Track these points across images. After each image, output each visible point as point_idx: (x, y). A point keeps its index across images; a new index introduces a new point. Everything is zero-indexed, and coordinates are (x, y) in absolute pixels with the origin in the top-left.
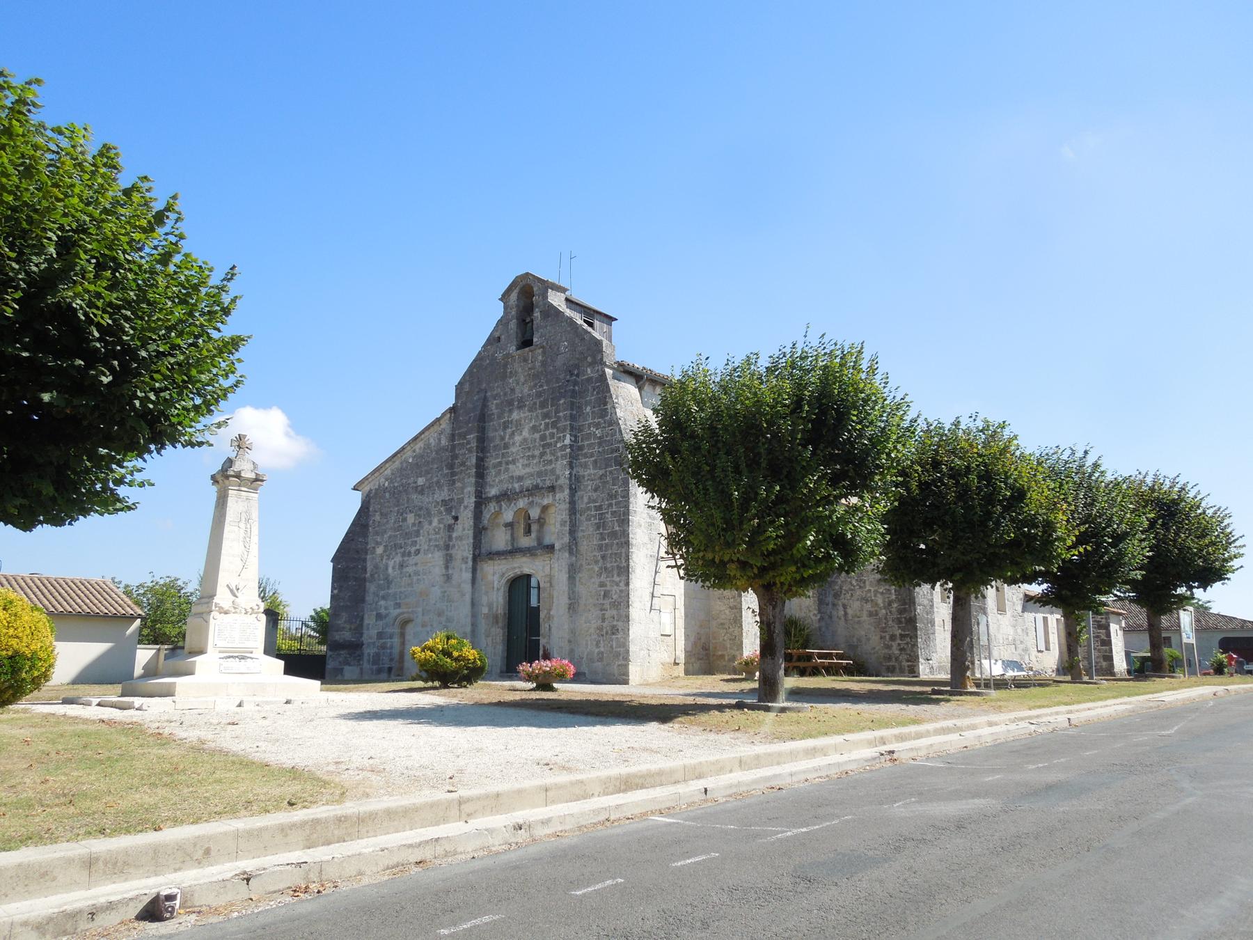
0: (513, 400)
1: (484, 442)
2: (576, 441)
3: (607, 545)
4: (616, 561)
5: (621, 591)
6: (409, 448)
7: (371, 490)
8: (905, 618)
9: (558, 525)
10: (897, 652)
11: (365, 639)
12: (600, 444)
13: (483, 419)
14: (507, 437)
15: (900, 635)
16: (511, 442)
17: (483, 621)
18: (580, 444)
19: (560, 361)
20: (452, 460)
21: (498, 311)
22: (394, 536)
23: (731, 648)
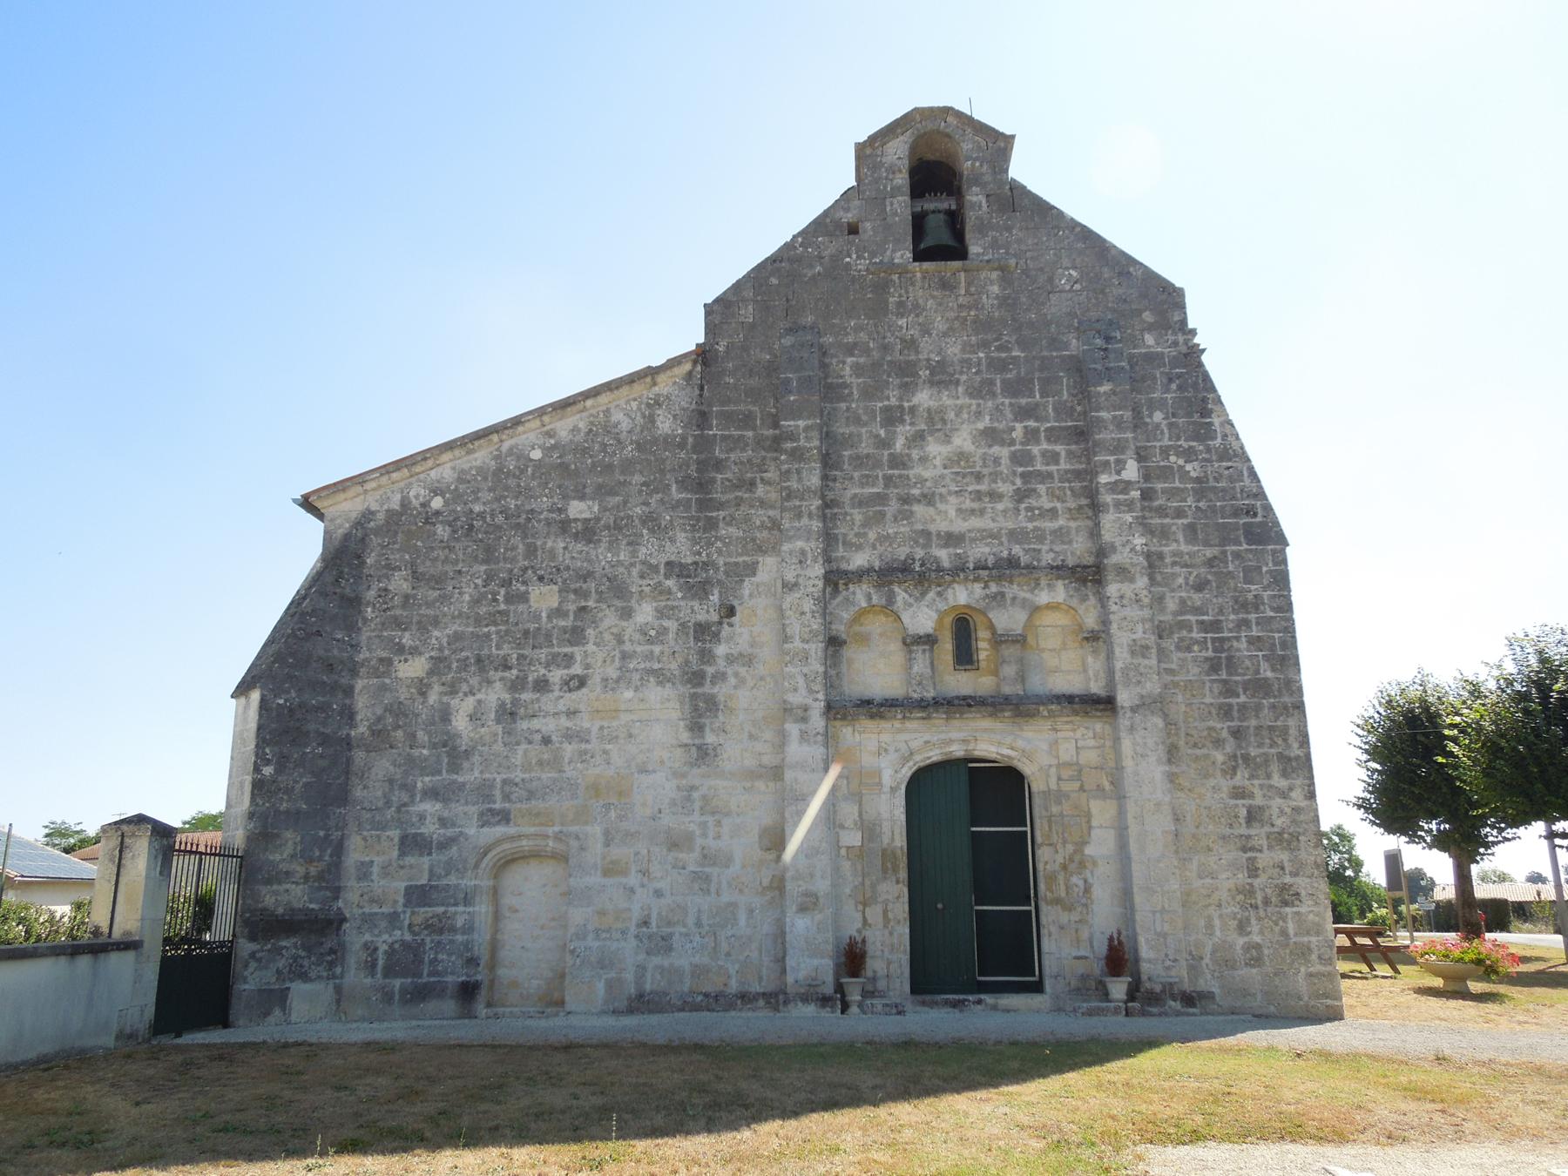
3: (1243, 708)
5: (1297, 810)
11: (352, 900)
16: (915, 454)
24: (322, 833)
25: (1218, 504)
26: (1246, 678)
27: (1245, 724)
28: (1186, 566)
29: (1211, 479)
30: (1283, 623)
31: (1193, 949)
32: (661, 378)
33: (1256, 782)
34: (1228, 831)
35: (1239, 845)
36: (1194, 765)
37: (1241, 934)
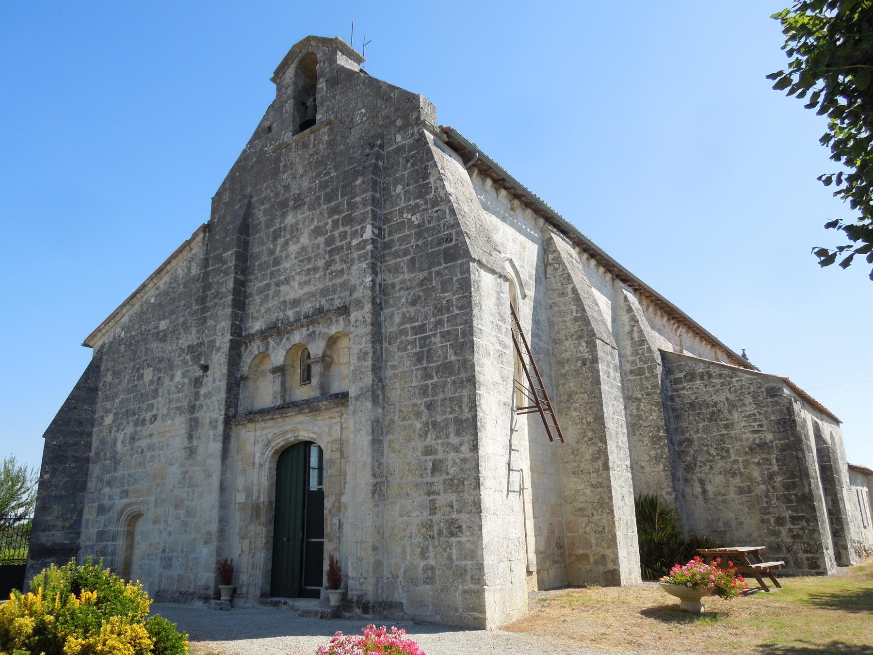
0: (287, 200)
1: (246, 261)
2: (380, 235)
3: (435, 386)
4: (452, 411)
5: (464, 460)
6: (151, 285)
7: (104, 344)
8: (796, 495)
9: (354, 360)
10: (789, 540)
11: (83, 541)
12: (419, 235)
13: (245, 229)
14: (279, 249)
15: (791, 517)
17: (238, 514)
18: (387, 239)
19: (354, 136)
20: (203, 292)
21: (270, 93)
22: (127, 399)
23: (597, 545)
24: (72, 506)
25: (429, 239)
26: (439, 363)
27: (435, 398)
28: (408, 289)
29: (426, 222)
30: (464, 317)
31: (393, 569)
32: (193, 245)
33: (439, 441)
34: (419, 480)
35: (425, 490)
36: (402, 433)
37: (422, 559)
